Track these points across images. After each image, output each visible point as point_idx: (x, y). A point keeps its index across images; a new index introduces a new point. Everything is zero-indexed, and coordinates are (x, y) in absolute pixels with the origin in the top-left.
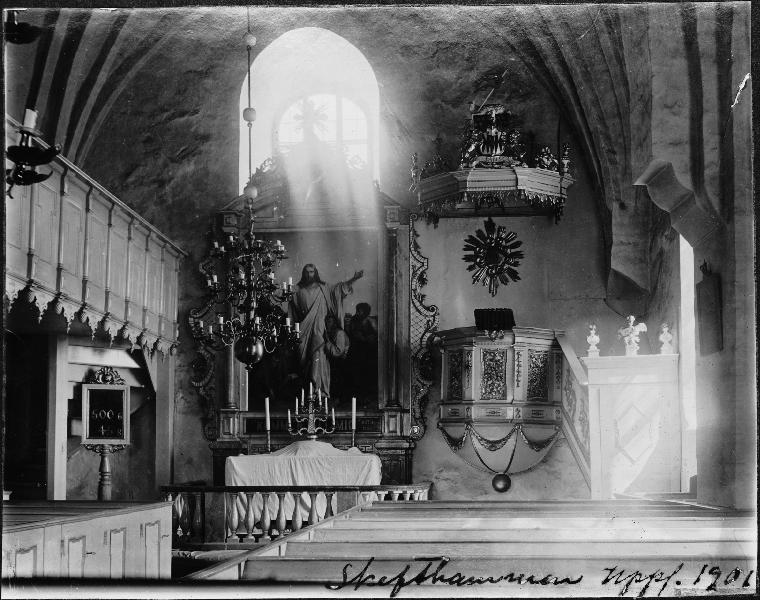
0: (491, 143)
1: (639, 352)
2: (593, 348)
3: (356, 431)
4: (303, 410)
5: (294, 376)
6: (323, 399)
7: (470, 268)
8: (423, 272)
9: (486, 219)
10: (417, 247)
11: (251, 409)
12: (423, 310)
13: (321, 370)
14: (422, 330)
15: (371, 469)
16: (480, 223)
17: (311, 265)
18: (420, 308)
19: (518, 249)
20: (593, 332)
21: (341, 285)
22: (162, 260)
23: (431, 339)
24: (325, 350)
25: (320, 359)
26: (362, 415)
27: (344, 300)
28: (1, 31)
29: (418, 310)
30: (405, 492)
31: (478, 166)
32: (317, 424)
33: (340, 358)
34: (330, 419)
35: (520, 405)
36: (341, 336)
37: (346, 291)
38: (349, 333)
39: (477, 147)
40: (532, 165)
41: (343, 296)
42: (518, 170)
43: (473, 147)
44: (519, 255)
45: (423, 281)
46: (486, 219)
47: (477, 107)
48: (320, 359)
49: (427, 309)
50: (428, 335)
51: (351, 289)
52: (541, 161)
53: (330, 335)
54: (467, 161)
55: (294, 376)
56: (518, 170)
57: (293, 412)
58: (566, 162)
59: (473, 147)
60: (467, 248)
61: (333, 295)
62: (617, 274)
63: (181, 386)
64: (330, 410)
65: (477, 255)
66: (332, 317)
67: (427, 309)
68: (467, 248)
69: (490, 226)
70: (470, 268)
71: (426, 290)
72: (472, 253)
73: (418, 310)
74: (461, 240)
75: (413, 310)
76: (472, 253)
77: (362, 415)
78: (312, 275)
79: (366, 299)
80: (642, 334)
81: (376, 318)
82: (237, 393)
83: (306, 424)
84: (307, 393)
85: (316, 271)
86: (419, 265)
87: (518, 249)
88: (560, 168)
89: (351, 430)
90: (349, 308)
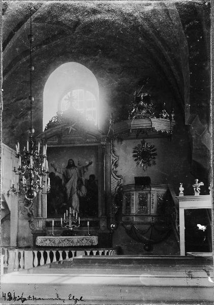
0: (141, 108)
1: (200, 194)
2: (181, 192)
3: (89, 226)
4: (67, 217)
5: (65, 204)
6: (75, 214)
7: (136, 160)
8: (117, 162)
9: (142, 140)
10: (114, 152)
11: (48, 218)
12: (115, 176)
13: (75, 203)
14: (116, 186)
15: (95, 239)
16: (139, 142)
17: (71, 160)
18: (115, 176)
19: (155, 152)
20: (181, 186)
21: (84, 167)
22: (11, 158)
23: (119, 189)
24: (77, 193)
25: (75, 198)
26: (56, 230)
27: (85, 173)
28: (213, 98)
29: (114, 177)
30: (104, 251)
31: (136, 118)
32: (73, 223)
33: (83, 197)
34: (78, 221)
35: (154, 216)
36: (83, 188)
37: (85, 170)
38: (87, 187)
39: (136, 110)
40: (158, 117)
41: (84, 172)
42: (152, 120)
43: (134, 110)
44: (156, 154)
45: (116, 165)
46: (142, 140)
47: (137, 93)
48: (75, 198)
49: (118, 177)
50: (118, 187)
51: (87, 169)
52: (162, 115)
53: (79, 188)
54: (132, 116)
55: (65, 204)
56: (152, 120)
57: (63, 218)
58: (173, 115)
59: (134, 110)
60: (134, 152)
61: (80, 171)
62: (194, 161)
63: (20, 209)
64: (78, 218)
65: (138, 154)
66: (80, 180)
67: (118, 177)
68: (134, 152)
69: (143, 143)
70: (136, 160)
71: (118, 169)
72: (136, 154)
73: (114, 177)
74: (131, 149)
75: (112, 177)
76: (136, 154)
77: (56, 230)
78: (72, 163)
79: (92, 173)
80: (201, 187)
81: (97, 181)
82: (42, 211)
83: (68, 223)
84: (69, 211)
85: (73, 162)
86: (114, 159)
87: (155, 152)
88: (170, 118)
89: (87, 226)
90: (86, 177)
